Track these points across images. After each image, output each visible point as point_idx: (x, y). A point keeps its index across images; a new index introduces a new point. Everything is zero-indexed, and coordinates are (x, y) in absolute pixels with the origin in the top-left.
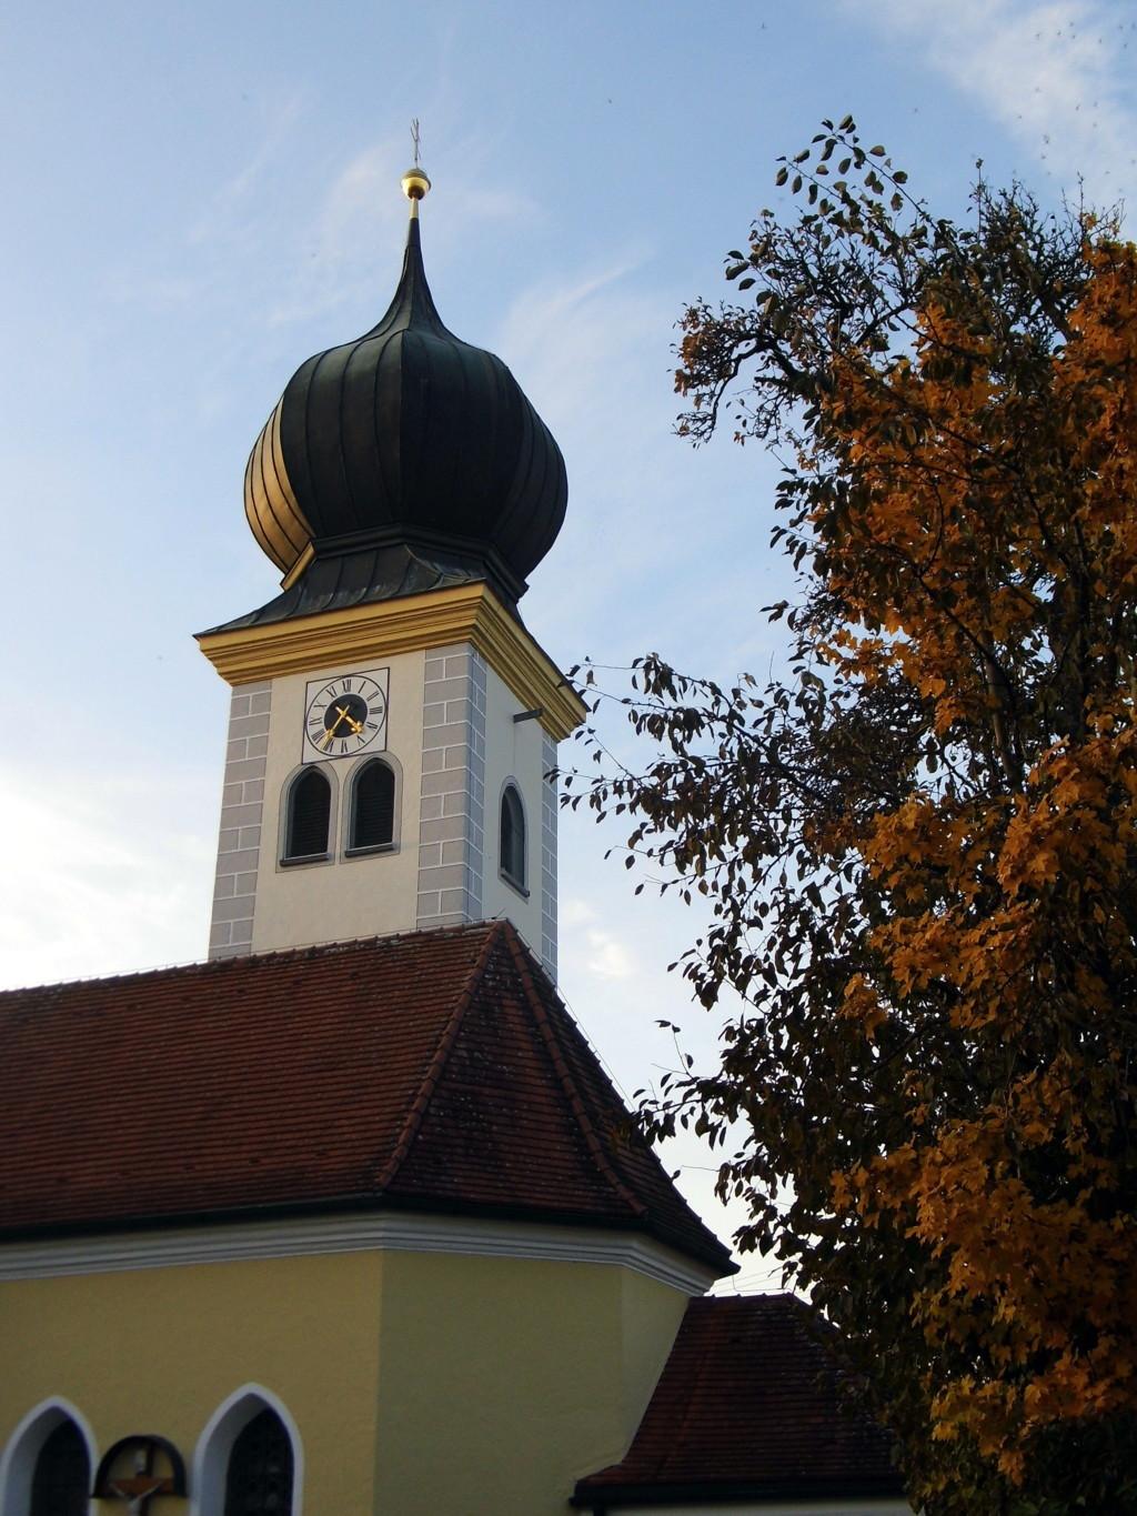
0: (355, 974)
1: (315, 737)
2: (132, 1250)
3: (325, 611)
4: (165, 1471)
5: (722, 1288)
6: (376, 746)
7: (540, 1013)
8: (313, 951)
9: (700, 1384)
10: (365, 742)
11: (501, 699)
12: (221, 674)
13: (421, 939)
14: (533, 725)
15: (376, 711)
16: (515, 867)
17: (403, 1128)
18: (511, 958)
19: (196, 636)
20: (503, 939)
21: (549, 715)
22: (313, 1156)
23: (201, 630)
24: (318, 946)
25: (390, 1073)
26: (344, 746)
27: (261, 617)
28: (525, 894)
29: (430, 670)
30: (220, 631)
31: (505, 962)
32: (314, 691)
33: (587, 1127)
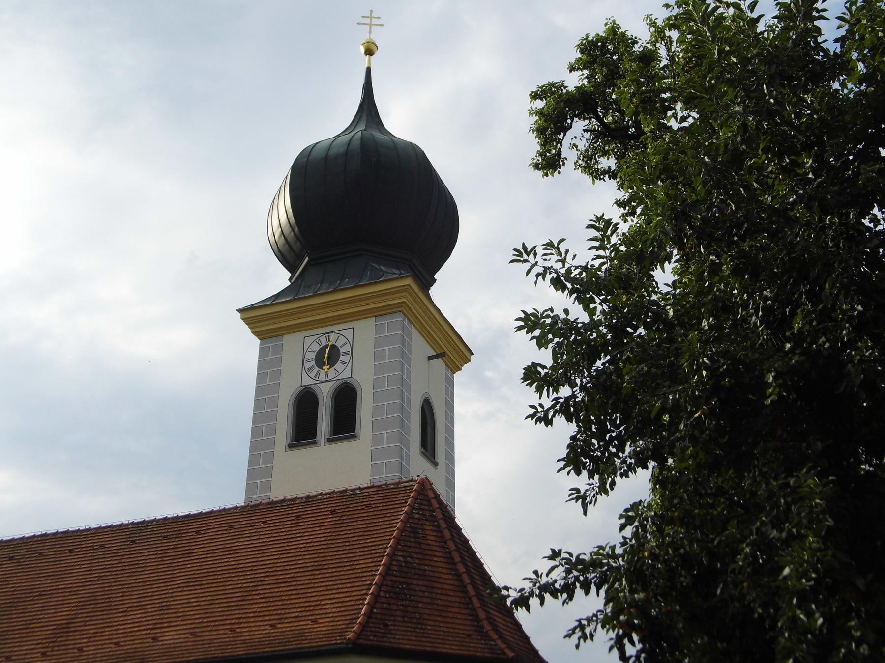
0: (334, 511)
1: (309, 369)
6: (346, 374)
7: (447, 533)
10: (340, 372)
11: (420, 348)
12: (253, 333)
14: (439, 361)
15: (346, 353)
16: (429, 447)
18: (429, 501)
20: (425, 486)
30: (252, 308)
31: (425, 502)
33: (476, 602)
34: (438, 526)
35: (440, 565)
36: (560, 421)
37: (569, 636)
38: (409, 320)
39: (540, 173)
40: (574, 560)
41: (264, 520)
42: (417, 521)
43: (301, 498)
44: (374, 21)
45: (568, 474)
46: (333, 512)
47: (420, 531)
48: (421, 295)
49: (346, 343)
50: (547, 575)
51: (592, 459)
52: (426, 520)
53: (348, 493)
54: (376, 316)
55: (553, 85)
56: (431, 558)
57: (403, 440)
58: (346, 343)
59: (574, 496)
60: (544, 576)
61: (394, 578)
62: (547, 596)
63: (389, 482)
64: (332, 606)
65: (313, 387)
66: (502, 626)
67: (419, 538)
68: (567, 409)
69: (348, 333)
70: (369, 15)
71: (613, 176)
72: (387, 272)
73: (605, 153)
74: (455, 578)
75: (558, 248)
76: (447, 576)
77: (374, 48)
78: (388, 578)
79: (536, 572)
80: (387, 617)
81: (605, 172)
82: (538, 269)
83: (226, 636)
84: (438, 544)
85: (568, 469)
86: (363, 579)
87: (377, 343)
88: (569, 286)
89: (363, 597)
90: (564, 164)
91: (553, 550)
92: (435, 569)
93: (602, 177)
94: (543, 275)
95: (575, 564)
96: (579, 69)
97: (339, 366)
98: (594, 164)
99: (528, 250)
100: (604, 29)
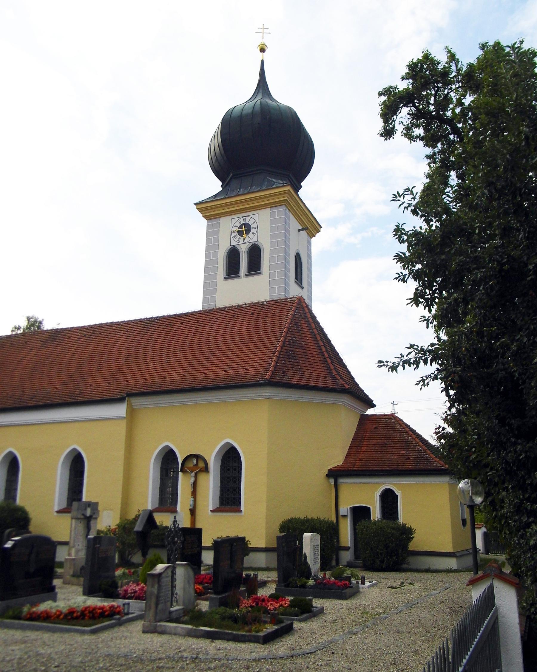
0: (253, 313)
1: (234, 237)
2: (262, 393)
3: (237, 195)
4: (201, 465)
5: (370, 412)
6: (254, 240)
7: (313, 325)
8: (238, 306)
9: (365, 441)
10: (252, 238)
11: (295, 225)
12: (203, 216)
14: (304, 232)
15: (254, 228)
16: (299, 277)
17: (273, 361)
18: (303, 308)
20: (300, 300)
22: (244, 370)
23: (196, 202)
24: (240, 304)
25: (267, 344)
28: (302, 288)
29: (272, 215)
30: (202, 202)
31: (301, 309)
32: (236, 221)
33: (329, 361)
34: (309, 321)
35: (310, 341)
36: (411, 281)
37: (418, 384)
38: (288, 209)
39: (384, 138)
40: (419, 349)
41: (216, 317)
42: (297, 319)
43: (235, 306)
44: (265, 31)
45: (412, 306)
47: (299, 324)
49: (254, 223)
50: (407, 356)
51: (425, 299)
53: (260, 303)
54: (271, 207)
55: (391, 87)
56: (305, 338)
57: (286, 275)
58: (254, 223)
59: (423, 319)
60: (405, 356)
61: (287, 348)
62: (407, 366)
63: (281, 298)
64: (255, 362)
65: (237, 246)
66: (341, 372)
67: (299, 328)
68: (417, 276)
69: (255, 217)
70: (262, 27)
71: (422, 139)
72: (276, 182)
73: (418, 126)
74: (318, 348)
75: (412, 192)
76: (313, 347)
77: (265, 48)
78: (284, 348)
79: (401, 355)
80: (285, 368)
81: (417, 137)
82: (406, 205)
83: (202, 376)
84: (308, 331)
85: (412, 303)
86: (271, 348)
87: (271, 222)
88: (420, 213)
89: (272, 357)
90: (396, 133)
91: (410, 344)
92: (307, 344)
93: (415, 140)
94: (406, 208)
95: (423, 351)
96: (407, 79)
97: (250, 235)
98: (411, 133)
99: (400, 194)
100: (422, 55)
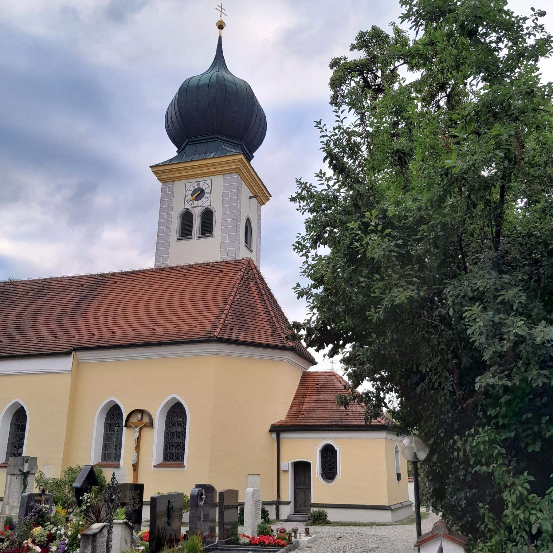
0: (204, 273)
3: (191, 161)
4: (146, 420)
5: (312, 369)
6: (207, 204)
11: (246, 192)
12: (158, 179)
13: (224, 263)
16: (248, 243)
19: (151, 167)
21: (260, 198)
24: (192, 264)
26: (197, 203)
27: (170, 162)
28: (252, 251)
29: (224, 181)
32: (190, 186)
43: (187, 266)
46: (203, 273)
48: (247, 164)
49: (208, 188)
52: (251, 279)
53: (211, 264)
58: (208, 188)
63: (231, 260)
69: (209, 182)
77: (224, 25)
97: (204, 199)
